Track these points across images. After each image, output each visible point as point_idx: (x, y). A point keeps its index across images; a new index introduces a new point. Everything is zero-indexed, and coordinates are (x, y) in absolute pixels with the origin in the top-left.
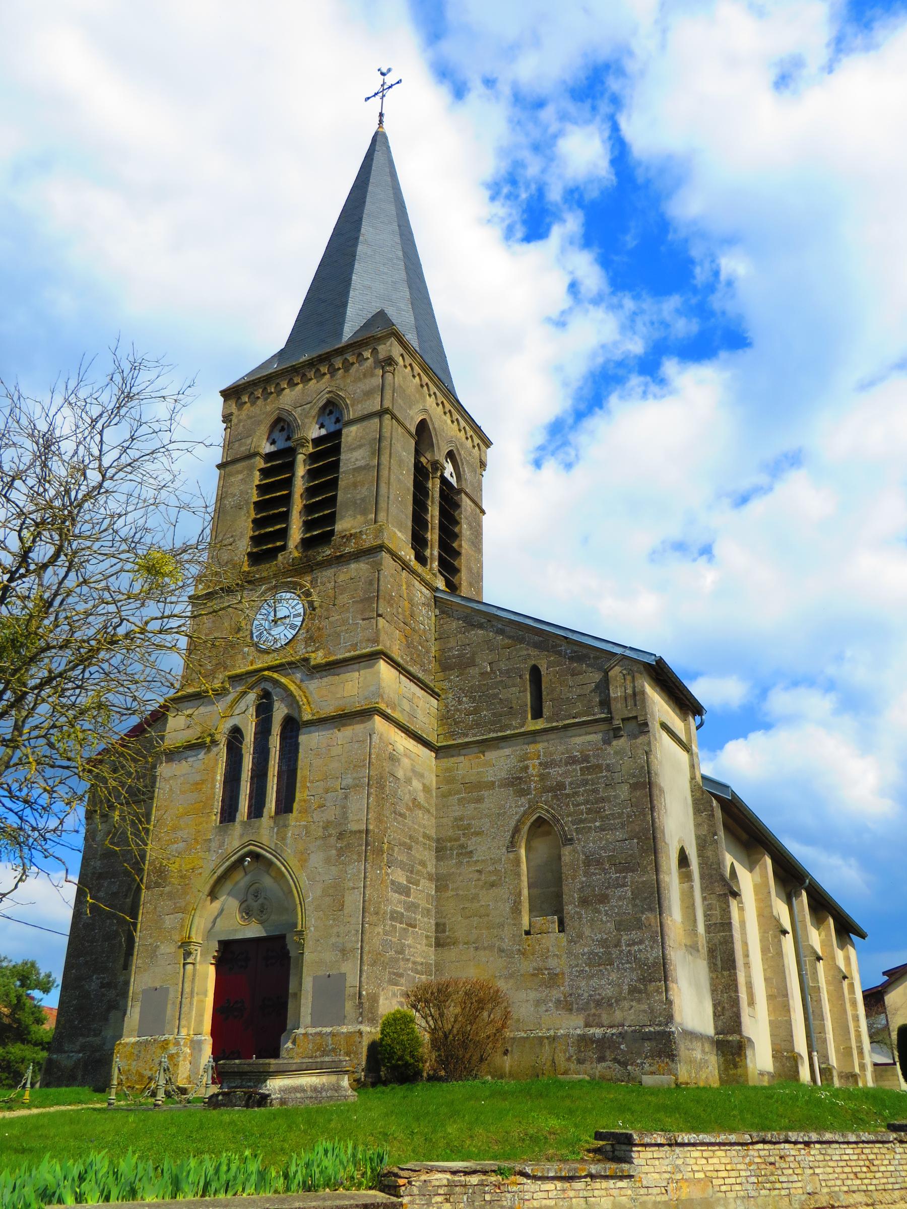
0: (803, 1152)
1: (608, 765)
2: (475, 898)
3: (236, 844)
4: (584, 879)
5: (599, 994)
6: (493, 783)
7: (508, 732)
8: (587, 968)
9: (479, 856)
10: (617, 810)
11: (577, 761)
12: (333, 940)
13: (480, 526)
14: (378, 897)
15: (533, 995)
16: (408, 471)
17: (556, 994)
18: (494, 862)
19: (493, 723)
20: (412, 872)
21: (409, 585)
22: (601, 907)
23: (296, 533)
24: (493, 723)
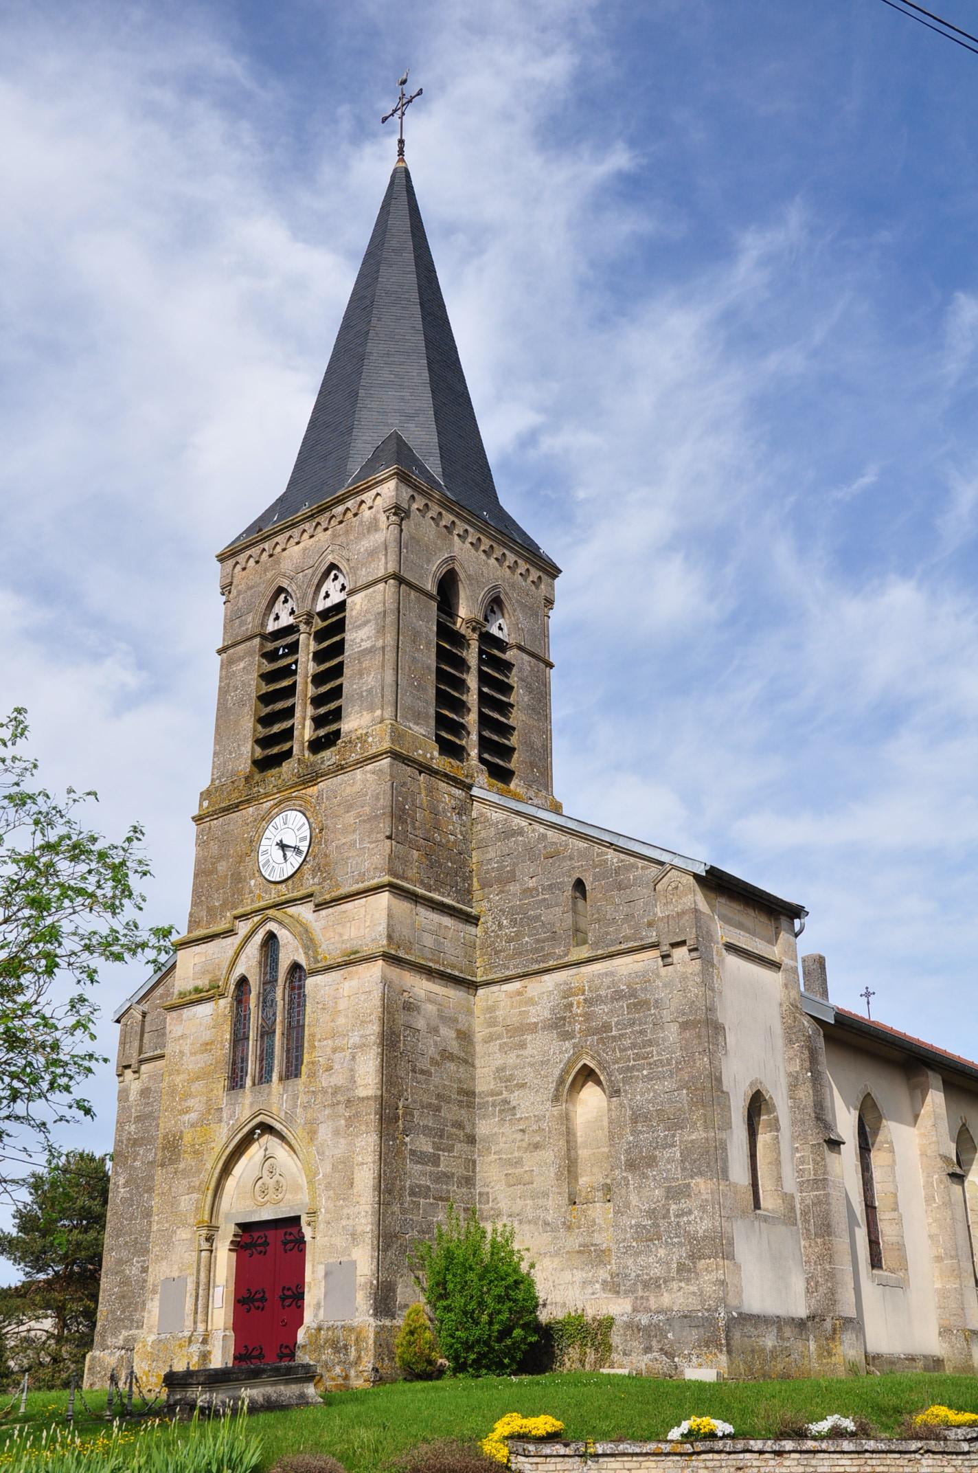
0: (772, 1463)
2: (518, 1163)
3: (247, 1114)
5: (647, 1274)
6: (536, 1024)
7: (551, 963)
8: (634, 1244)
10: (665, 1056)
11: (624, 996)
12: (344, 1222)
13: (545, 684)
14: (392, 1172)
15: (579, 1275)
16: (428, 644)
17: (603, 1274)
18: (539, 1119)
19: (536, 951)
20: (441, 1137)
21: (430, 790)
23: (305, 731)
24: (536, 951)
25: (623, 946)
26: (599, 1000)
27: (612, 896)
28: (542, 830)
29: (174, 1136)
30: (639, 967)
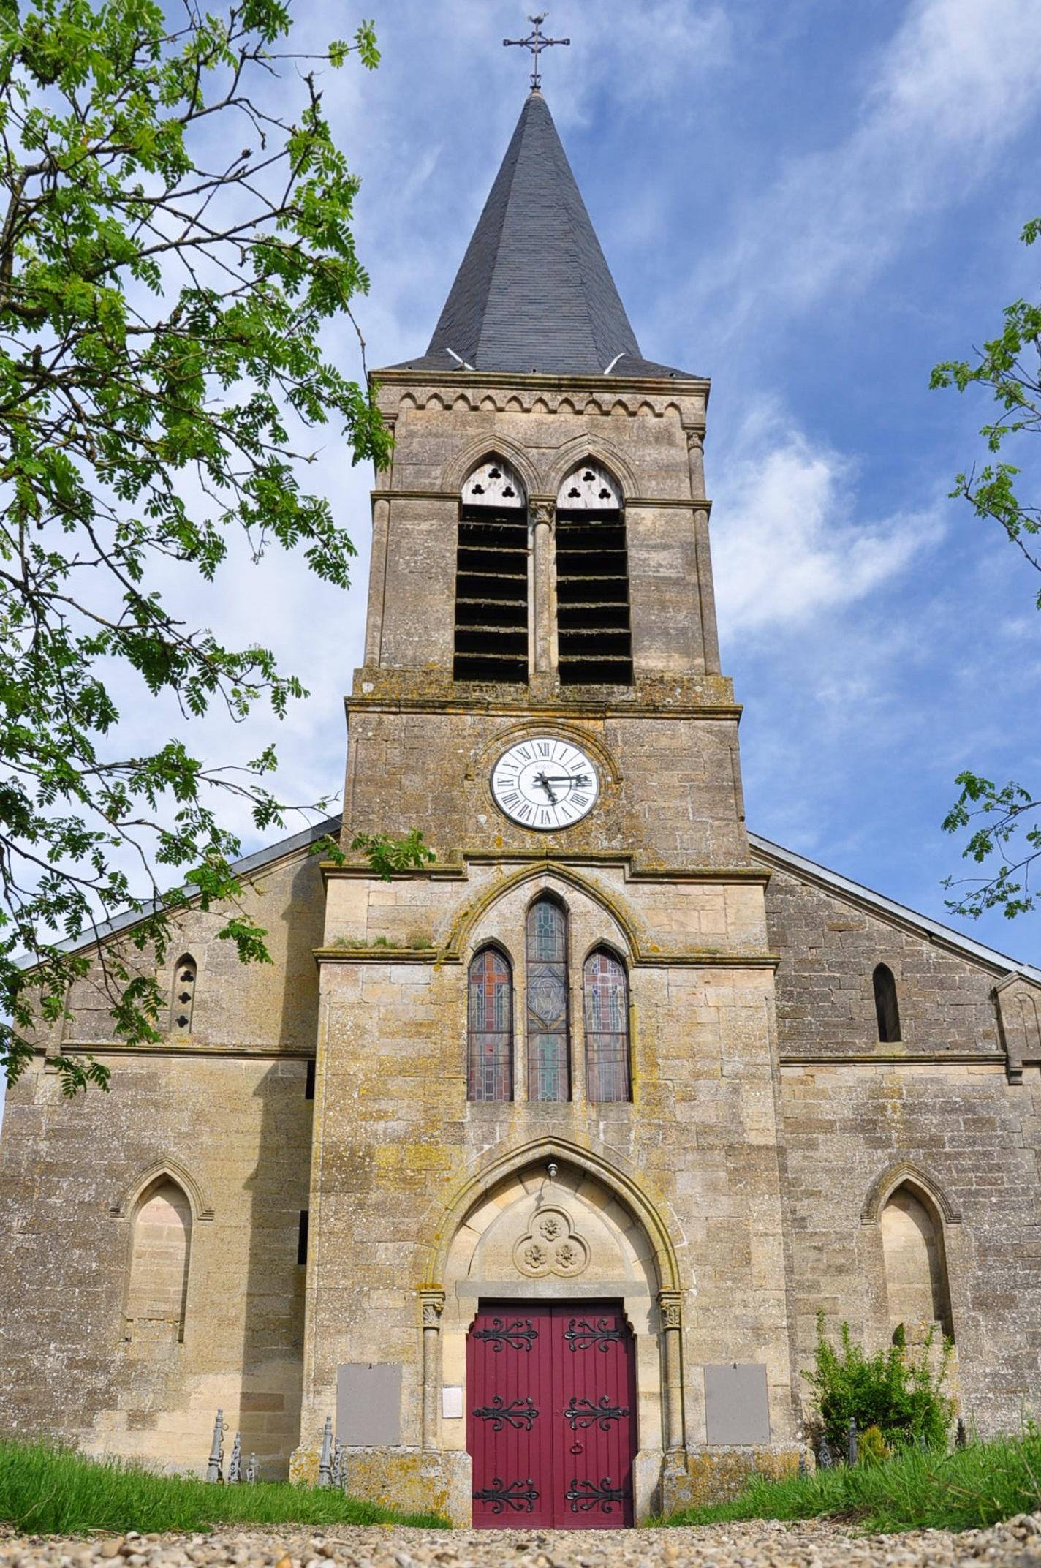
1: (1003, 1122)
4: (980, 1273)
6: (832, 1124)
9: (815, 1227)
10: (1020, 1185)
18: (841, 1237)
22: (1006, 1313)
24: (825, 1035)
25: (949, 1053)
26: (923, 1108)
27: (931, 994)
28: (823, 896)
29: (353, 1155)
30: (976, 1080)
